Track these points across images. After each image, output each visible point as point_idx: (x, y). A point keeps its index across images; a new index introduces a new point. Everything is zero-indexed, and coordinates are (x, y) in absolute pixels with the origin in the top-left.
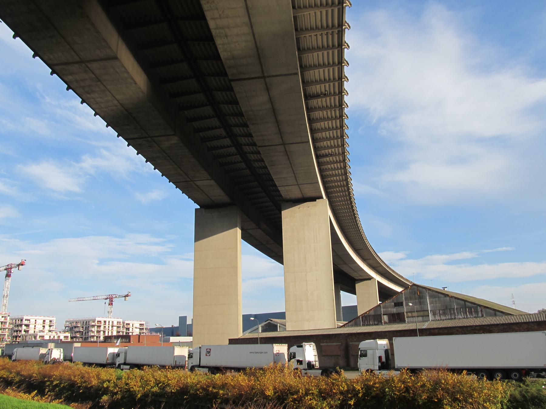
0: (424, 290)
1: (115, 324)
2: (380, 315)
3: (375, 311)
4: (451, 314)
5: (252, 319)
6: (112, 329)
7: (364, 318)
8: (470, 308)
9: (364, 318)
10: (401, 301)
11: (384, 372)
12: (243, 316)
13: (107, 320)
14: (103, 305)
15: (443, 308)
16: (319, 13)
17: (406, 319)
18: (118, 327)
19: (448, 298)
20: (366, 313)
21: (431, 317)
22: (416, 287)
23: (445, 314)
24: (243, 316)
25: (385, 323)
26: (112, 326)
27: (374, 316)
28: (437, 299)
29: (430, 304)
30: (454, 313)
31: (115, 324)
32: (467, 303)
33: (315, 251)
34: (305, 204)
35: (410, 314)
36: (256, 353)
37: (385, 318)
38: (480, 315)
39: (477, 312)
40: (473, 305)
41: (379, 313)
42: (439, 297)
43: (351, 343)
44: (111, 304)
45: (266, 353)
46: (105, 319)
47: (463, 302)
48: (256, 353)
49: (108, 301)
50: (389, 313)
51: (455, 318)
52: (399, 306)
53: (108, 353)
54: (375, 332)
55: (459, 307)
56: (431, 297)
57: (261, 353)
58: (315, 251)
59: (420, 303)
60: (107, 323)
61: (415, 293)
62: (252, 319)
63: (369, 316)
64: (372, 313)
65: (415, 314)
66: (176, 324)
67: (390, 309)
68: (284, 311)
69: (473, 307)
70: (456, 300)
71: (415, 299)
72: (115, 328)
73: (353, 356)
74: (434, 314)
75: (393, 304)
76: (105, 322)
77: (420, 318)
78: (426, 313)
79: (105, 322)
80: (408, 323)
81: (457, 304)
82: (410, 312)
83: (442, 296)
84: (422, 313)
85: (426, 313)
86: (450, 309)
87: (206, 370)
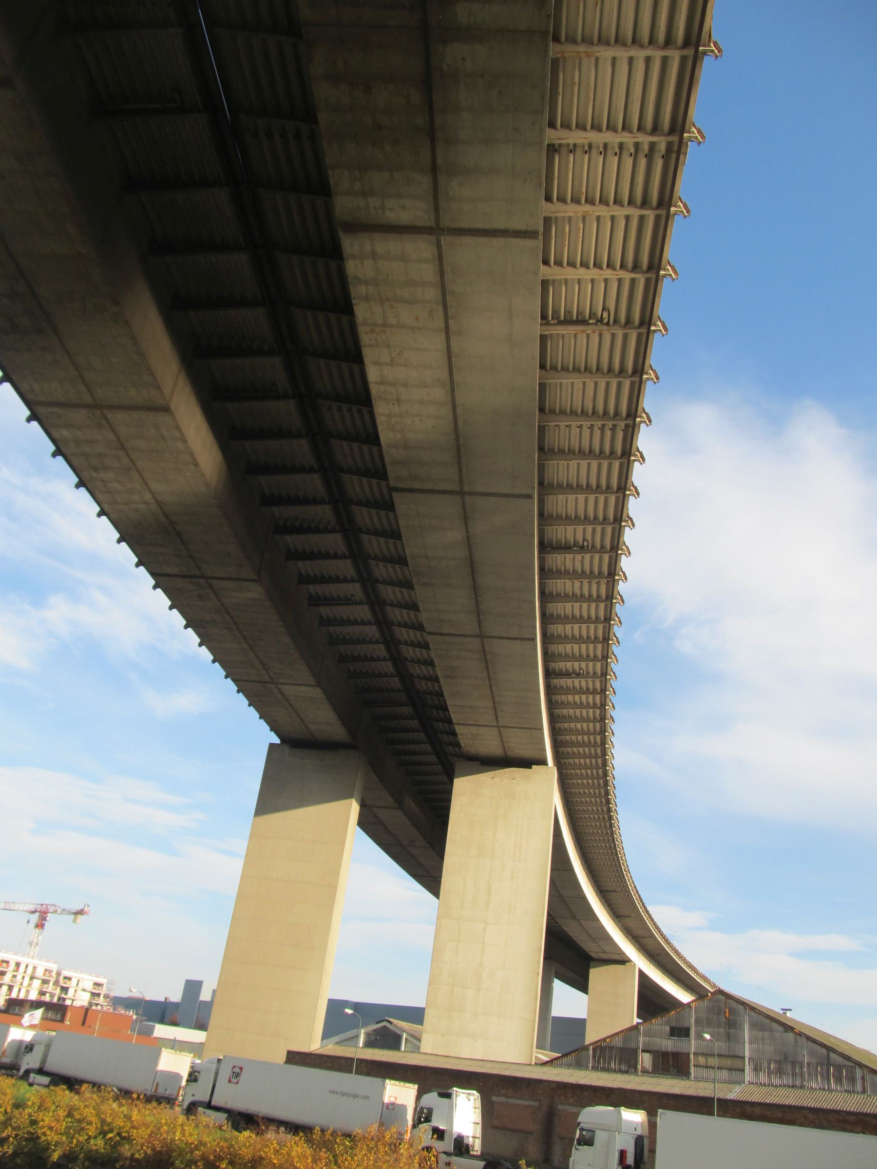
0: (741, 1007)
1: (40, 973)
2: (634, 1052)
3: (625, 1040)
4: (794, 1075)
6: (30, 985)
8: (839, 1068)
10: (686, 1025)
13: (24, 960)
14: (24, 924)
18: (45, 982)
19: (791, 1036)
23: (780, 1072)
25: (645, 1071)
26: (32, 978)
27: (622, 1050)
28: (767, 1034)
29: (750, 1043)
31: (40, 973)
32: (832, 1055)
35: (701, 1060)
37: (645, 1060)
38: (859, 1087)
39: (852, 1080)
40: (846, 1063)
43: (560, 1107)
44: (40, 925)
46: (19, 959)
47: (824, 1051)
49: (35, 918)
51: (802, 1087)
52: (679, 1036)
55: (814, 1060)
57: (356, 1096)
60: (22, 968)
62: (349, 1011)
67: (658, 1040)
70: (810, 1043)
71: (719, 1026)
72: (37, 983)
73: (562, 1138)
74: (756, 1069)
75: (668, 1028)
76: (18, 965)
77: (725, 1074)
78: (737, 1063)
79: (18, 965)
80: (697, 1079)
81: (812, 1053)
83: (780, 1028)
84: (728, 1062)
85: (737, 1063)
86: (793, 1063)
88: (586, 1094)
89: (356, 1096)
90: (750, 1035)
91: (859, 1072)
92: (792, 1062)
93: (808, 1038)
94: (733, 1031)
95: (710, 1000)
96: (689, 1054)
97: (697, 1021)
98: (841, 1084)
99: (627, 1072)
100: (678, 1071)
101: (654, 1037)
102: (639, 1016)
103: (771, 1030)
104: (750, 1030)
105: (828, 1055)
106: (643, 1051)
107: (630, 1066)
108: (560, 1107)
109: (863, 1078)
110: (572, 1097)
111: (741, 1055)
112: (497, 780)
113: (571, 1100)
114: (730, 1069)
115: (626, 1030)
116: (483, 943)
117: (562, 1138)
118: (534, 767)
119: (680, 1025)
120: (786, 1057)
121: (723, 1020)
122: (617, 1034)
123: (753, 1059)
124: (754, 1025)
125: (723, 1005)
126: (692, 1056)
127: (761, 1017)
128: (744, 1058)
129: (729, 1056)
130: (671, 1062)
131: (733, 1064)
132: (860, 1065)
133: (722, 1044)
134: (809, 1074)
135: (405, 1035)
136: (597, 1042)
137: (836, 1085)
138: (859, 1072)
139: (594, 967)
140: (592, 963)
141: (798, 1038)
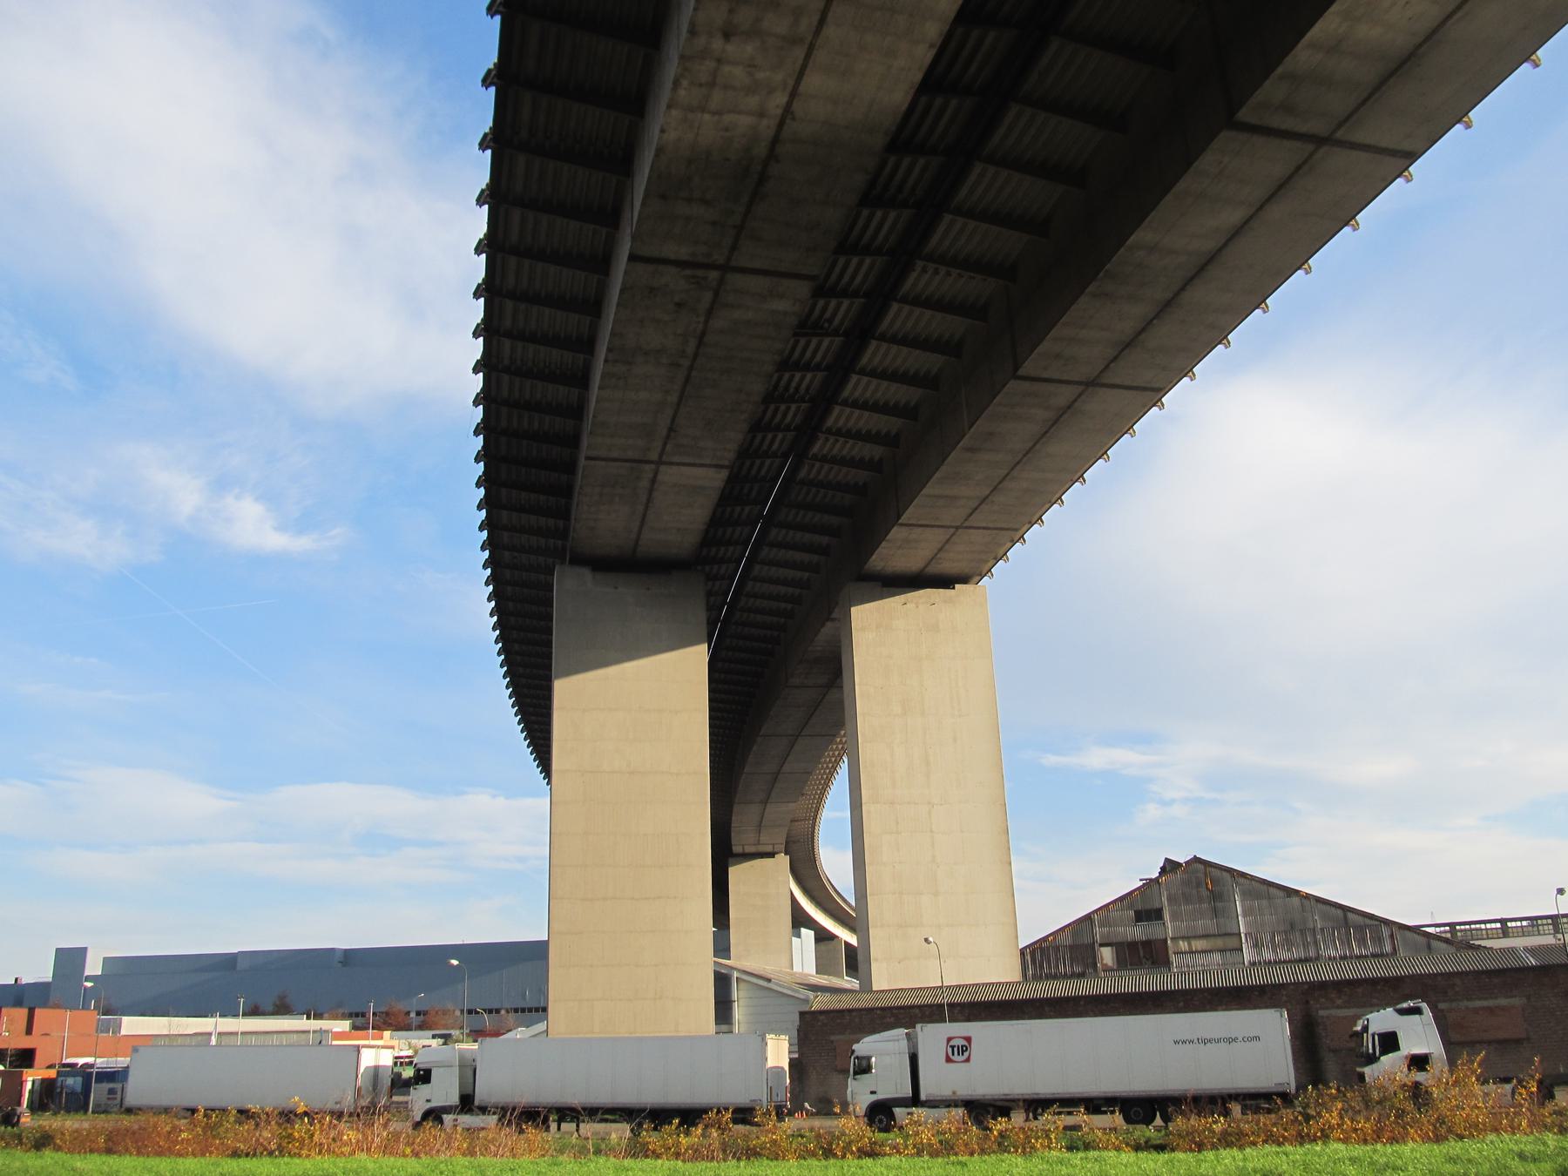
7: (1038, 956)
8: (1360, 929)
9: (1038, 956)
10: (1157, 906)
11: (740, 1127)
12: (60, 952)
17: (1173, 958)
19: (1295, 900)
20: (1045, 939)
21: (1248, 955)
22: (1201, 867)
24: (60, 952)
28: (1265, 902)
29: (1244, 916)
30: (1316, 943)
32: (1350, 915)
33: (955, 740)
34: (922, 592)
35: (1183, 945)
36: (1205, 1041)
37: (1107, 955)
40: (1368, 922)
41: (1087, 940)
42: (1269, 898)
43: (1321, 1013)
47: (1339, 912)
48: (1205, 1041)
50: (1119, 939)
53: (362, 1070)
56: (1244, 895)
58: (955, 740)
59: (1215, 913)
61: (1198, 885)
63: (1057, 948)
64: (1067, 940)
65: (1198, 944)
66: (45, 973)
67: (1121, 929)
68: (533, 930)
69: (1367, 926)
71: (1201, 900)
73: (1335, 1051)
74: (1257, 945)
75: (1132, 913)
78: (1231, 942)
81: (1324, 917)
82: (1183, 938)
83: (1281, 894)
84: (1219, 943)
85: (1231, 942)
86: (1303, 932)
87: (961, 1111)
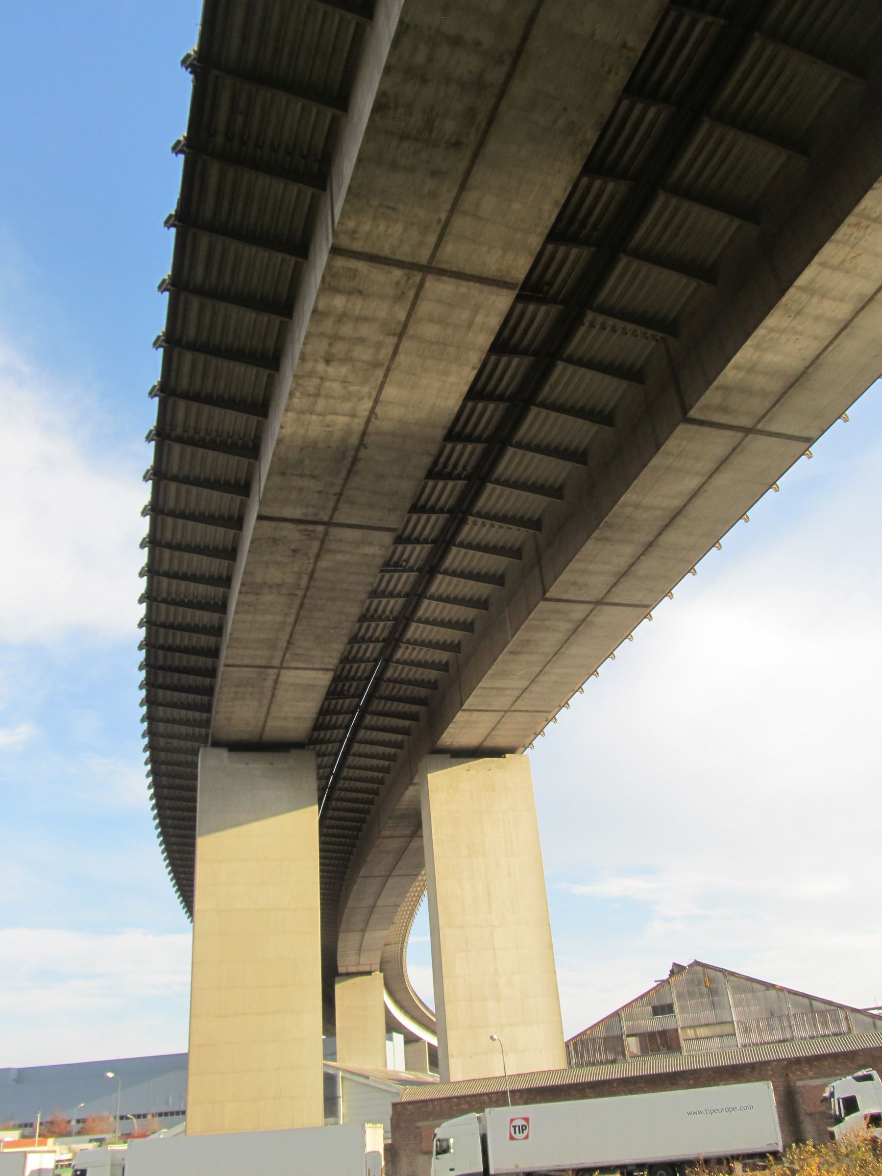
0: (720, 975)
2: (620, 1039)
3: (607, 1029)
4: (783, 1029)
5: (110, 1075)
7: (579, 1045)
8: (822, 1013)
10: (669, 1002)
15: (765, 1015)
16: (265, 379)
19: (773, 992)
27: (605, 1039)
28: (750, 995)
29: (735, 1007)
32: (814, 1003)
34: (481, 760)
35: (690, 1033)
37: (632, 1044)
40: (828, 1007)
41: (616, 1032)
43: (799, 1083)
45: (689, 1114)
47: (806, 1001)
52: (663, 1013)
54: (863, 1050)
55: (799, 1011)
57: (731, 1110)
61: (699, 984)
62: (110, 1075)
64: (601, 1033)
67: (642, 1022)
68: (184, 1050)
70: (792, 996)
71: (702, 995)
73: (811, 1115)
74: (746, 1030)
75: (650, 1009)
78: (727, 1029)
81: (795, 1004)
82: (690, 1027)
83: (762, 988)
84: (718, 1030)
85: (727, 1029)
86: (780, 1018)
88: (826, 1063)
89: (731, 1110)
90: (733, 998)
91: (841, 1014)
92: (779, 1017)
93: (790, 991)
94: (716, 999)
95: (688, 973)
96: (676, 1030)
97: (678, 996)
98: (827, 1029)
99: (614, 1062)
100: (668, 1049)
101: (638, 1019)
102: (324, 1034)
103: (753, 991)
104: (733, 995)
105: (811, 1005)
106: (628, 1036)
107: (617, 1053)
108: (799, 1083)
109: (846, 1018)
110: (811, 1070)
111: (730, 1020)
112: (473, 772)
113: (811, 1074)
114: (721, 1036)
115: (606, 1018)
116: (493, 949)
117: (811, 1115)
118: (507, 755)
119: (663, 1003)
120: (772, 1014)
121: (705, 990)
122: (597, 1024)
123: (741, 1022)
124: (736, 989)
125: (702, 976)
126: (679, 1031)
127: (741, 980)
128: (732, 1022)
129: (717, 1024)
130: (659, 1041)
131: (723, 1028)
132: (841, 1007)
133: (708, 1013)
134: (797, 1025)
135: (341, 1074)
136: (574, 1038)
137: (823, 1029)
138: (841, 1014)
139: (339, 982)
140: (337, 979)
141: (780, 993)
